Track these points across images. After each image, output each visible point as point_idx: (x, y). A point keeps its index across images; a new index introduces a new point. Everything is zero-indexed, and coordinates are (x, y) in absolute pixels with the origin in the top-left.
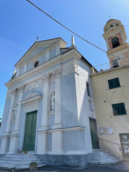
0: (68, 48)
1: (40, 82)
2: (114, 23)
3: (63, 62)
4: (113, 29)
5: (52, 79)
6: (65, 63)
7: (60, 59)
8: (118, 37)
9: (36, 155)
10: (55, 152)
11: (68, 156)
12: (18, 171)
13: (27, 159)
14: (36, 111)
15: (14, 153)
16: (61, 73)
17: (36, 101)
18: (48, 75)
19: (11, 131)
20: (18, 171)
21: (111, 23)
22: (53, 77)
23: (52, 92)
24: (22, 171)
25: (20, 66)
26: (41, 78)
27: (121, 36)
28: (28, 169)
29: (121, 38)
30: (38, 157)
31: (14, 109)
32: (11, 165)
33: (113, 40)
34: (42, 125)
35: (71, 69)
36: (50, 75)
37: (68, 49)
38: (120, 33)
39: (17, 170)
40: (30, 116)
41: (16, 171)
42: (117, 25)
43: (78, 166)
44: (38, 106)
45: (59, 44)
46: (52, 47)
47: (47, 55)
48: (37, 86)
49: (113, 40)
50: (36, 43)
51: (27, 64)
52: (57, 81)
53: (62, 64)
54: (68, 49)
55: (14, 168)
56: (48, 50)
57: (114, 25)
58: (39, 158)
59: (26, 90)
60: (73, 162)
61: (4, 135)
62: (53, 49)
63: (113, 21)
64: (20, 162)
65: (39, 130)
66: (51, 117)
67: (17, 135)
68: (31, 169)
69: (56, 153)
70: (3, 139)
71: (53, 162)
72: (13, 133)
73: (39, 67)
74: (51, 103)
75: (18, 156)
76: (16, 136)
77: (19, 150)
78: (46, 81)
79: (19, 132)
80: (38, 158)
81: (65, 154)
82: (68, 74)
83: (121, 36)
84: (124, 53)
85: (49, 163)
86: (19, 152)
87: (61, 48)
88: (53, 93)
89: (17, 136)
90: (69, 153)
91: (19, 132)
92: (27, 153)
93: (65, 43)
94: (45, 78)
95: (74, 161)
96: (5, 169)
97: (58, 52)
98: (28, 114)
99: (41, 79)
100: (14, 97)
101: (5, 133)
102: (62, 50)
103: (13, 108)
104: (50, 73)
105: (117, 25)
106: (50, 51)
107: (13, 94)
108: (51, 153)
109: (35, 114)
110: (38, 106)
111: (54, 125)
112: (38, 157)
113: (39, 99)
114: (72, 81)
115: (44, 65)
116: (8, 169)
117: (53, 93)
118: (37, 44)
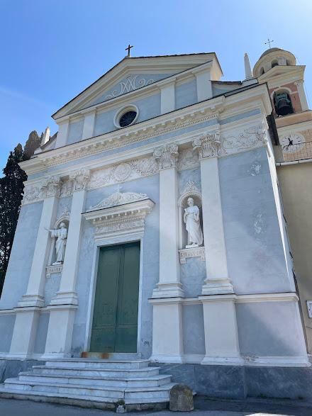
0: (240, 83)
1: (146, 165)
2: (281, 59)
3: (223, 117)
4: (279, 72)
5: (184, 160)
6: (228, 121)
7: (217, 108)
8: (291, 93)
9: (151, 365)
10: (217, 357)
11: (265, 369)
12: (135, 411)
13: (138, 374)
14: (137, 244)
15: (65, 356)
16: (218, 146)
17: (105, 221)
18: (89, 171)
19: (44, 293)
20: (135, 411)
21: (273, 56)
22: (189, 155)
23: (191, 196)
24: (143, 411)
25: (70, 118)
26: (151, 155)
27: (296, 92)
28: (166, 406)
29: (296, 96)
30: (160, 370)
31: (54, 233)
32: (97, 393)
33: (278, 97)
34: (62, 290)
35: (254, 137)
36: (182, 150)
37: (237, 87)
38: (296, 84)
39: (131, 407)
40: (112, 257)
41: (128, 412)
42: (288, 65)
43: (301, 398)
44: (143, 229)
45: (208, 70)
46: (101, 107)
47: (167, 98)
48: (260, 157)
49: (278, 97)
50: (128, 61)
51: (94, 115)
52: (209, 168)
53: (220, 122)
54: (237, 87)
55: (122, 403)
56: (65, 120)
57: (282, 62)
58: (165, 373)
59: (93, 183)
60: (281, 386)
61: (22, 304)
62: (184, 82)
63: (280, 52)
64: (123, 384)
65: (154, 294)
66: (189, 261)
67: (73, 307)
68: (180, 404)
69: (223, 360)
70: (19, 317)
71: (216, 387)
72: (55, 301)
73: (133, 127)
74: (184, 225)
75: (99, 365)
76: (71, 309)
77: (77, 350)
78: (167, 165)
79: (76, 297)
80: (161, 372)
81: (250, 364)
82: (241, 151)
83: (296, 92)
84: (304, 133)
85: (204, 388)
86: (80, 354)
87: (213, 82)
88: (190, 199)
89: (74, 309)
90: (262, 362)
91: (76, 297)
92: (110, 357)
93: (219, 70)
94: (166, 156)
95: (289, 384)
96: (82, 403)
97: (204, 91)
98: (103, 249)
99: (152, 158)
100: (53, 199)
101: (25, 299)
102: (217, 86)
103: (52, 231)
104: (181, 143)
105: (288, 65)
106: (175, 88)
107: (52, 193)
108: (207, 360)
109: (129, 253)
110: (143, 229)
111: (205, 284)
112: (160, 370)
113: (146, 210)
114: (258, 168)
115: (153, 124)
116: (95, 404)
117: (190, 199)
118: (129, 63)
